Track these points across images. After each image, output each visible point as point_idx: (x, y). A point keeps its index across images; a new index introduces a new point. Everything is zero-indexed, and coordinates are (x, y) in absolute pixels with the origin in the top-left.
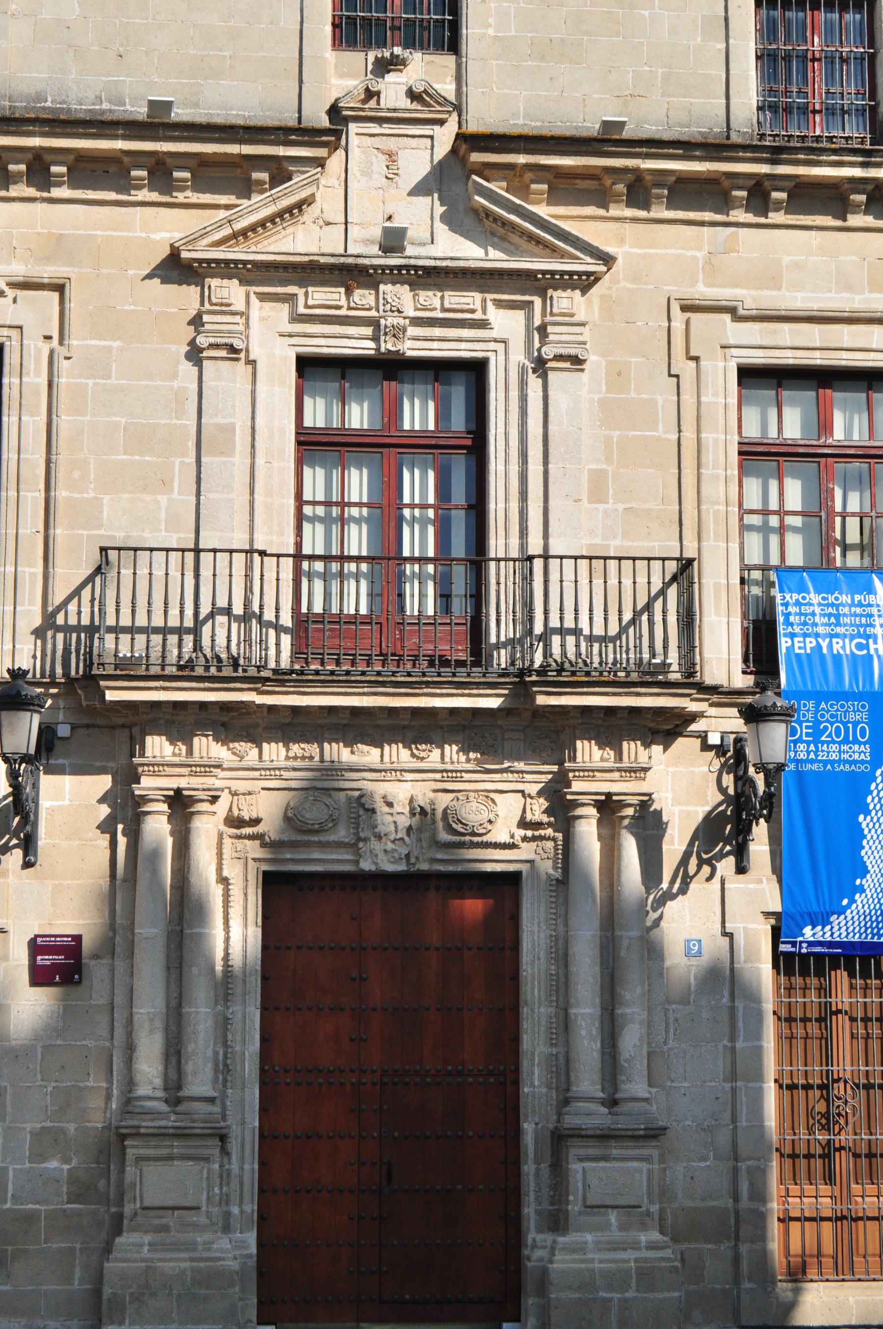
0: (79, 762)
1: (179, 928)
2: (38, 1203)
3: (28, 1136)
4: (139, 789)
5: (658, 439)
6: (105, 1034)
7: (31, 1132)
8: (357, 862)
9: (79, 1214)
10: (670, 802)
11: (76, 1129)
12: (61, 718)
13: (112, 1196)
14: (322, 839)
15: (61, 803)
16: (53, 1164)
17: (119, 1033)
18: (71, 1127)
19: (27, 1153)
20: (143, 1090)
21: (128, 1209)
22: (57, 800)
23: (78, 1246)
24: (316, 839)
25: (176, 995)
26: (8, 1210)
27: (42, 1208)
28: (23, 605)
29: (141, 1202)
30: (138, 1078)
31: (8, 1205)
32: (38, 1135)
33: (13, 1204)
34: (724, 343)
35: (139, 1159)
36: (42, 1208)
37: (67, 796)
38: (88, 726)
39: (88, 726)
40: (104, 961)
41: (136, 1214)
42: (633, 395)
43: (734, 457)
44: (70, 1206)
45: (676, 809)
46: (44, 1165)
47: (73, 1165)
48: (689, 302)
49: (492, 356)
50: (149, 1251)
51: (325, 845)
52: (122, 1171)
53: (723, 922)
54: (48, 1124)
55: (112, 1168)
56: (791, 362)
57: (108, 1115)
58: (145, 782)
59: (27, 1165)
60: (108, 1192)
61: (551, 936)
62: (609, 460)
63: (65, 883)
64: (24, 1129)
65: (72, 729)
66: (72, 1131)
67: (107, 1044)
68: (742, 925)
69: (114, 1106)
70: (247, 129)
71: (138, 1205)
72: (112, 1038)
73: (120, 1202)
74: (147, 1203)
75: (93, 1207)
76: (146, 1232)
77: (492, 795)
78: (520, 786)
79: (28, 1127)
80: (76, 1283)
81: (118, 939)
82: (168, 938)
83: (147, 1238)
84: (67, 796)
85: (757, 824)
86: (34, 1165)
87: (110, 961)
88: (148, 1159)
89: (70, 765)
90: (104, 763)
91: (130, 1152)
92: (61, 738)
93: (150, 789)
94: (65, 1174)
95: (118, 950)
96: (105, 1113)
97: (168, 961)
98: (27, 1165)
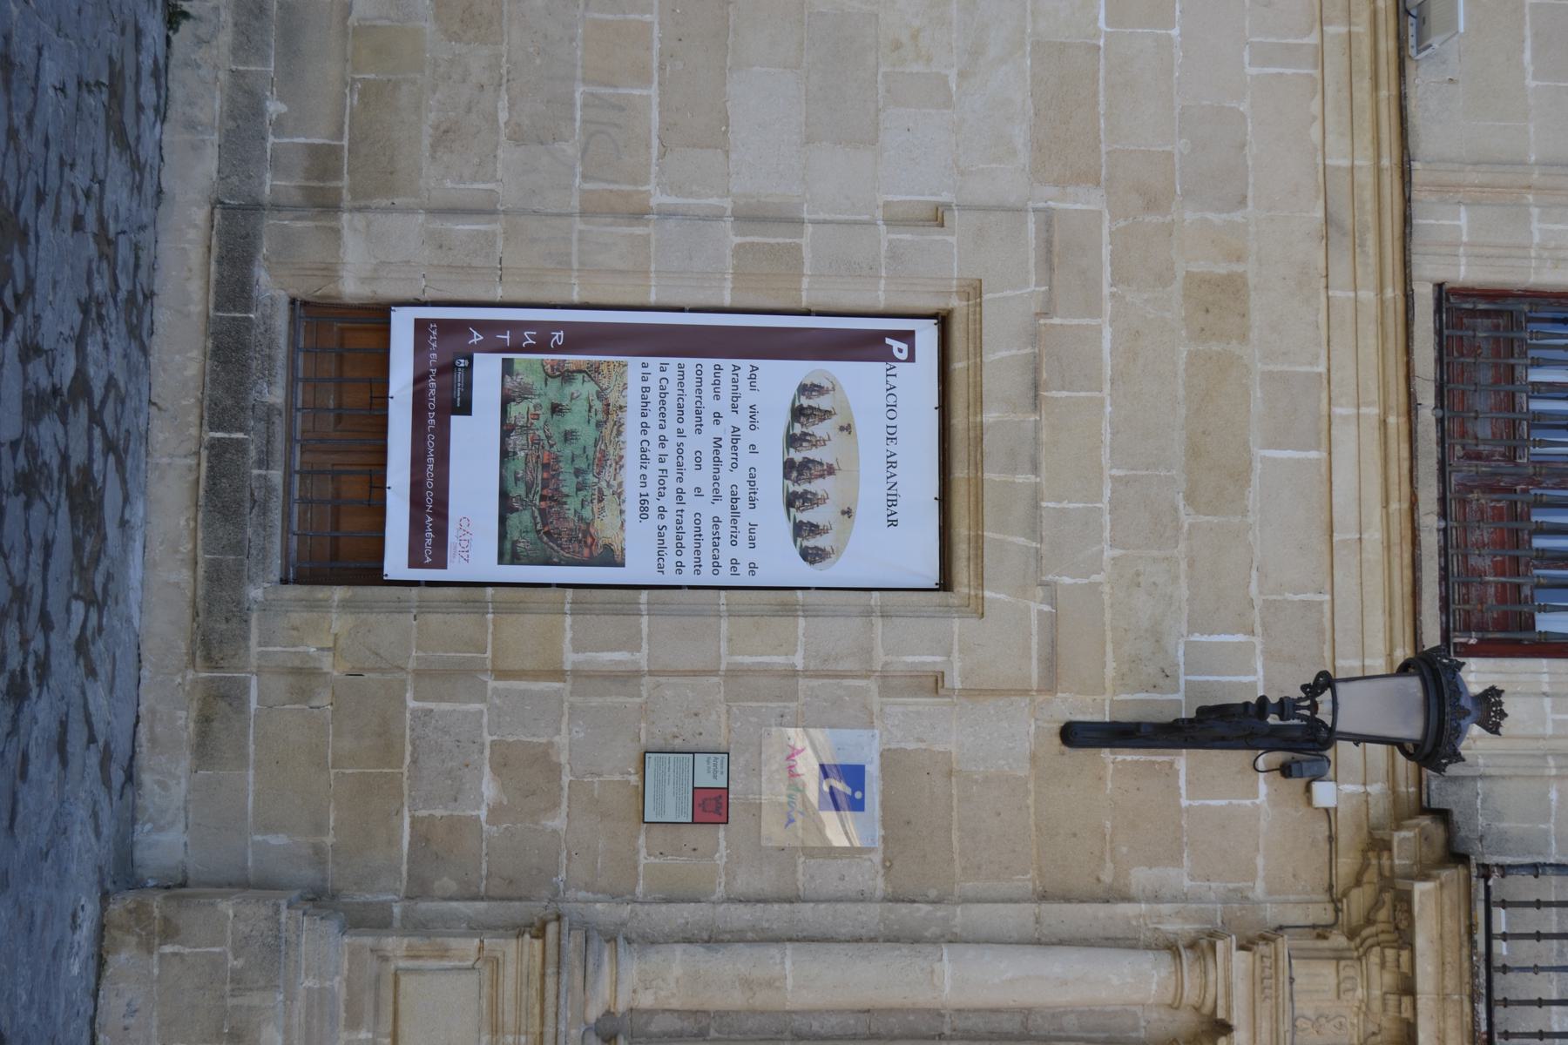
0: (1263, 825)
1: (947, 1032)
2: (414, 762)
3: (544, 740)
4: (1228, 950)
6: (742, 884)
7: (551, 744)
9: (393, 841)
11: (555, 831)
12: (1348, 788)
13: (423, 906)
15: (1183, 792)
16: (489, 789)
17: (743, 915)
18: (558, 822)
19: (510, 739)
20: (632, 967)
21: (394, 944)
22: (1189, 782)
23: (329, 840)
25: (816, 1026)
26: (404, 702)
27: (405, 769)
28: (1555, 709)
29: (407, 970)
30: (655, 957)
31: (412, 704)
32: (544, 761)
33: (413, 711)
35: (496, 963)
36: (405, 769)
37: (1196, 803)
38: (1332, 839)
39: (1332, 839)
40: (880, 883)
41: (385, 959)
44: (407, 821)
46: (487, 769)
47: (485, 827)
50: (309, 990)
52: (476, 928)
54: (566, 779)
55: (481, 905)
57: (582, 894)
58: (1241, 960)
59: (488, 739)
60: (432, 898)
63: (1030, 801)
64: (558, 731)
65: (1327, 810)
66: (550, 823)
67: (720, 891)
69: (598, 906)
70: (1092, 945)
71: (402, 964)
72: (729, 900)
73: (419, 927)
74: (404, 980)
75: (404, 868)
76: (349, 982)
79: (562, 739)
80: (258, 838)
81: (925, 908)
82: (929, 1011)
83: (338, 984)
84: (1196, 803)
85: (76, 410)
86: (487, 752)
87: (879, 894)
88: (495, 984)
89: (1257, 807)
90: (1261, 873)
91: (509, 948)
92: (1308, 789)
93: (1228, 971)
94: (469, 813)
95: (904, 909)
96: (587, 888)
97: (881, 1011)
98: (488, 739)
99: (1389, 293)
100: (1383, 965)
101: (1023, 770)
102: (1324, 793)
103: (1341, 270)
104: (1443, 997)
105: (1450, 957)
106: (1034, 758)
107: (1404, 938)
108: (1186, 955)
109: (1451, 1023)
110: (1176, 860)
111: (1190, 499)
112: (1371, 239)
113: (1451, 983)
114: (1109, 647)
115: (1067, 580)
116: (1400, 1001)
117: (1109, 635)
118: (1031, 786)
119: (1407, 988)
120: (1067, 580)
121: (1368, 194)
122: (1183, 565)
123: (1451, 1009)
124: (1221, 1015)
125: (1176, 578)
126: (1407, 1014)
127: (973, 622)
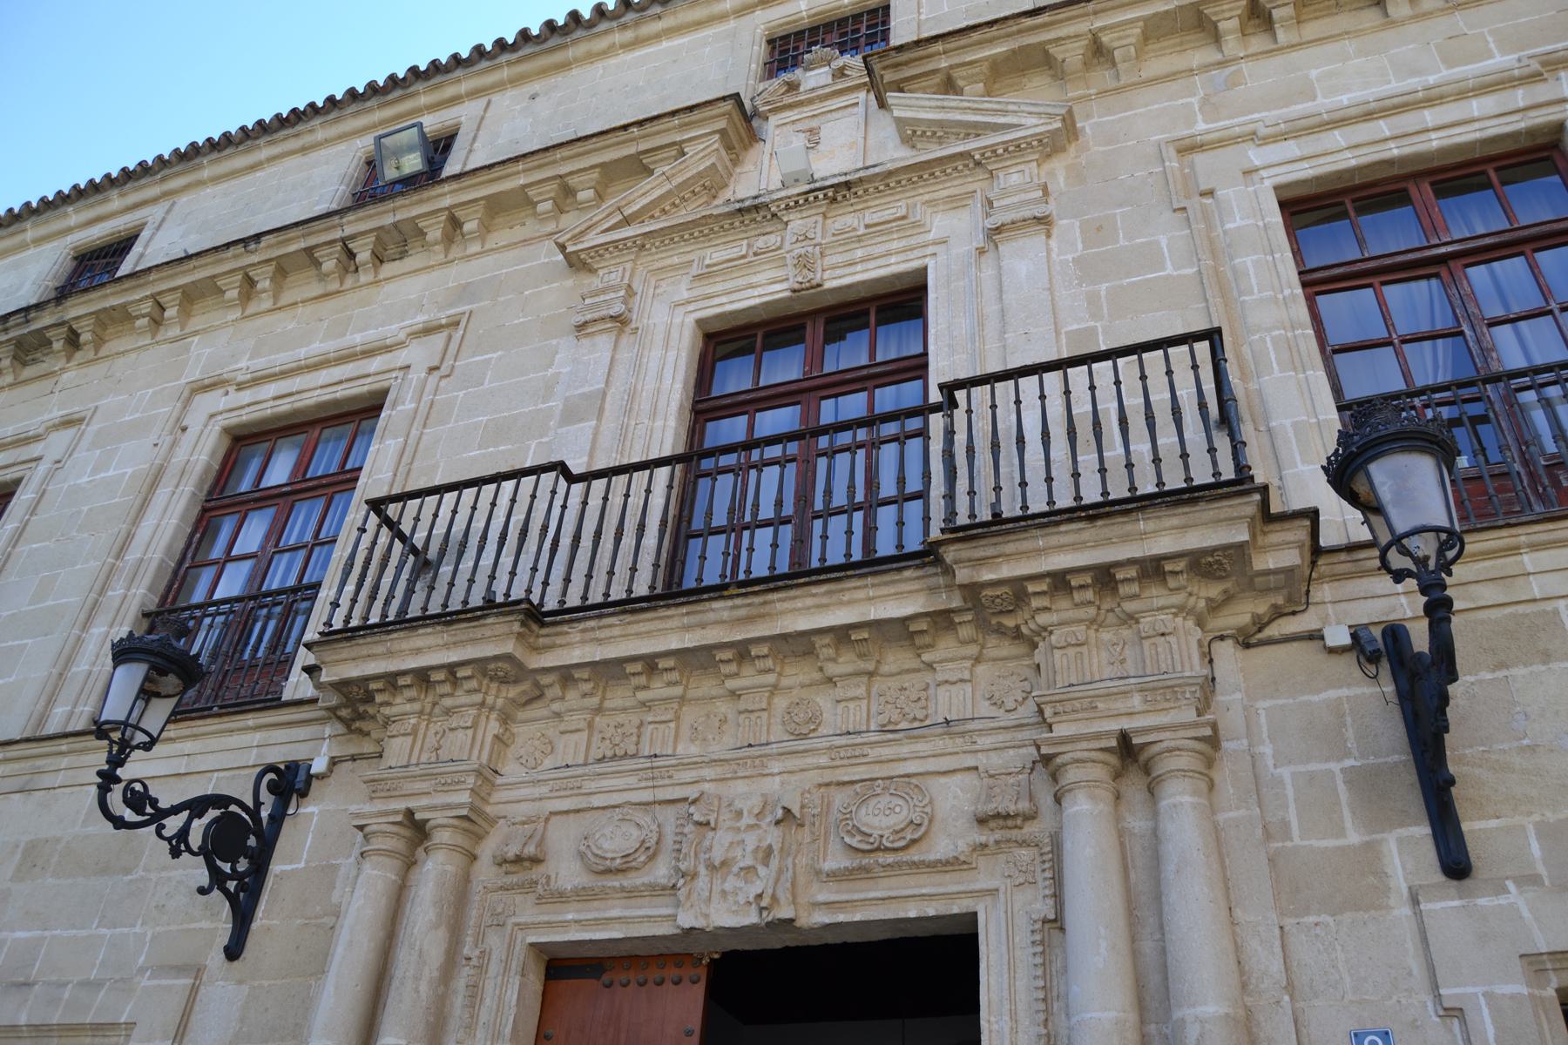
5: (1169, 276)
8: (674, 917)
10: (1270, 762)
14: (625, 883)
24: (617, 884)
34: (1247, 166)
38: (353, 758)
39: (353, 758)
42: (1123, 242)
43: (1276, 218)
45: (1285, 772)
48: (1187, 142)
49: (930, 263)
51: (630, 893)
53: (1435, 987)
56: (1349, 161)
58: (1061, 730)
61: (1039, 1036)
62: (1095, 316)
63: (266, 983)
68: (1479, 990)
77: (914, 781)
78: (970, 761)
99: (64, 748)
100: (388, 704)
101: (245, 989)
102: (319, 766)
103: (47, 780)
104: (390, 654)
105: (364, 651)
106: (240, 982)
107: (1018, 590)
108: (1063, 782)
109: (405, 645)
110: (335, 868)
111: (127, 871)
112: (39, 762)
113: (379, 649)
114: (192, 926)
115: (142, 958)
116: (1123, 581)
117: (185, 926)
118: (256, 984)
119: (1060, 581)
120: (142, 958)
121: (16, 766)
122: (164, 874)
123: (396, 646)
124: (1114, 743)
125: (169, 879)
126: (1087, 579)
127: (136, 1030)
